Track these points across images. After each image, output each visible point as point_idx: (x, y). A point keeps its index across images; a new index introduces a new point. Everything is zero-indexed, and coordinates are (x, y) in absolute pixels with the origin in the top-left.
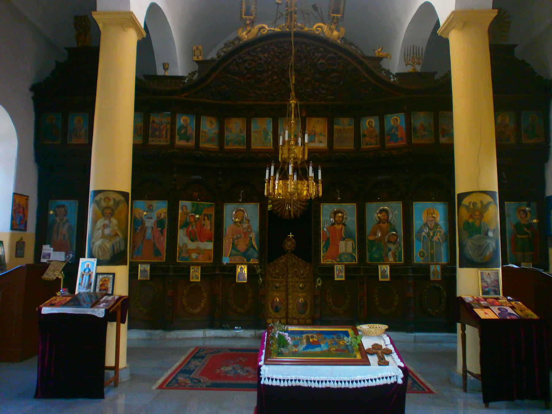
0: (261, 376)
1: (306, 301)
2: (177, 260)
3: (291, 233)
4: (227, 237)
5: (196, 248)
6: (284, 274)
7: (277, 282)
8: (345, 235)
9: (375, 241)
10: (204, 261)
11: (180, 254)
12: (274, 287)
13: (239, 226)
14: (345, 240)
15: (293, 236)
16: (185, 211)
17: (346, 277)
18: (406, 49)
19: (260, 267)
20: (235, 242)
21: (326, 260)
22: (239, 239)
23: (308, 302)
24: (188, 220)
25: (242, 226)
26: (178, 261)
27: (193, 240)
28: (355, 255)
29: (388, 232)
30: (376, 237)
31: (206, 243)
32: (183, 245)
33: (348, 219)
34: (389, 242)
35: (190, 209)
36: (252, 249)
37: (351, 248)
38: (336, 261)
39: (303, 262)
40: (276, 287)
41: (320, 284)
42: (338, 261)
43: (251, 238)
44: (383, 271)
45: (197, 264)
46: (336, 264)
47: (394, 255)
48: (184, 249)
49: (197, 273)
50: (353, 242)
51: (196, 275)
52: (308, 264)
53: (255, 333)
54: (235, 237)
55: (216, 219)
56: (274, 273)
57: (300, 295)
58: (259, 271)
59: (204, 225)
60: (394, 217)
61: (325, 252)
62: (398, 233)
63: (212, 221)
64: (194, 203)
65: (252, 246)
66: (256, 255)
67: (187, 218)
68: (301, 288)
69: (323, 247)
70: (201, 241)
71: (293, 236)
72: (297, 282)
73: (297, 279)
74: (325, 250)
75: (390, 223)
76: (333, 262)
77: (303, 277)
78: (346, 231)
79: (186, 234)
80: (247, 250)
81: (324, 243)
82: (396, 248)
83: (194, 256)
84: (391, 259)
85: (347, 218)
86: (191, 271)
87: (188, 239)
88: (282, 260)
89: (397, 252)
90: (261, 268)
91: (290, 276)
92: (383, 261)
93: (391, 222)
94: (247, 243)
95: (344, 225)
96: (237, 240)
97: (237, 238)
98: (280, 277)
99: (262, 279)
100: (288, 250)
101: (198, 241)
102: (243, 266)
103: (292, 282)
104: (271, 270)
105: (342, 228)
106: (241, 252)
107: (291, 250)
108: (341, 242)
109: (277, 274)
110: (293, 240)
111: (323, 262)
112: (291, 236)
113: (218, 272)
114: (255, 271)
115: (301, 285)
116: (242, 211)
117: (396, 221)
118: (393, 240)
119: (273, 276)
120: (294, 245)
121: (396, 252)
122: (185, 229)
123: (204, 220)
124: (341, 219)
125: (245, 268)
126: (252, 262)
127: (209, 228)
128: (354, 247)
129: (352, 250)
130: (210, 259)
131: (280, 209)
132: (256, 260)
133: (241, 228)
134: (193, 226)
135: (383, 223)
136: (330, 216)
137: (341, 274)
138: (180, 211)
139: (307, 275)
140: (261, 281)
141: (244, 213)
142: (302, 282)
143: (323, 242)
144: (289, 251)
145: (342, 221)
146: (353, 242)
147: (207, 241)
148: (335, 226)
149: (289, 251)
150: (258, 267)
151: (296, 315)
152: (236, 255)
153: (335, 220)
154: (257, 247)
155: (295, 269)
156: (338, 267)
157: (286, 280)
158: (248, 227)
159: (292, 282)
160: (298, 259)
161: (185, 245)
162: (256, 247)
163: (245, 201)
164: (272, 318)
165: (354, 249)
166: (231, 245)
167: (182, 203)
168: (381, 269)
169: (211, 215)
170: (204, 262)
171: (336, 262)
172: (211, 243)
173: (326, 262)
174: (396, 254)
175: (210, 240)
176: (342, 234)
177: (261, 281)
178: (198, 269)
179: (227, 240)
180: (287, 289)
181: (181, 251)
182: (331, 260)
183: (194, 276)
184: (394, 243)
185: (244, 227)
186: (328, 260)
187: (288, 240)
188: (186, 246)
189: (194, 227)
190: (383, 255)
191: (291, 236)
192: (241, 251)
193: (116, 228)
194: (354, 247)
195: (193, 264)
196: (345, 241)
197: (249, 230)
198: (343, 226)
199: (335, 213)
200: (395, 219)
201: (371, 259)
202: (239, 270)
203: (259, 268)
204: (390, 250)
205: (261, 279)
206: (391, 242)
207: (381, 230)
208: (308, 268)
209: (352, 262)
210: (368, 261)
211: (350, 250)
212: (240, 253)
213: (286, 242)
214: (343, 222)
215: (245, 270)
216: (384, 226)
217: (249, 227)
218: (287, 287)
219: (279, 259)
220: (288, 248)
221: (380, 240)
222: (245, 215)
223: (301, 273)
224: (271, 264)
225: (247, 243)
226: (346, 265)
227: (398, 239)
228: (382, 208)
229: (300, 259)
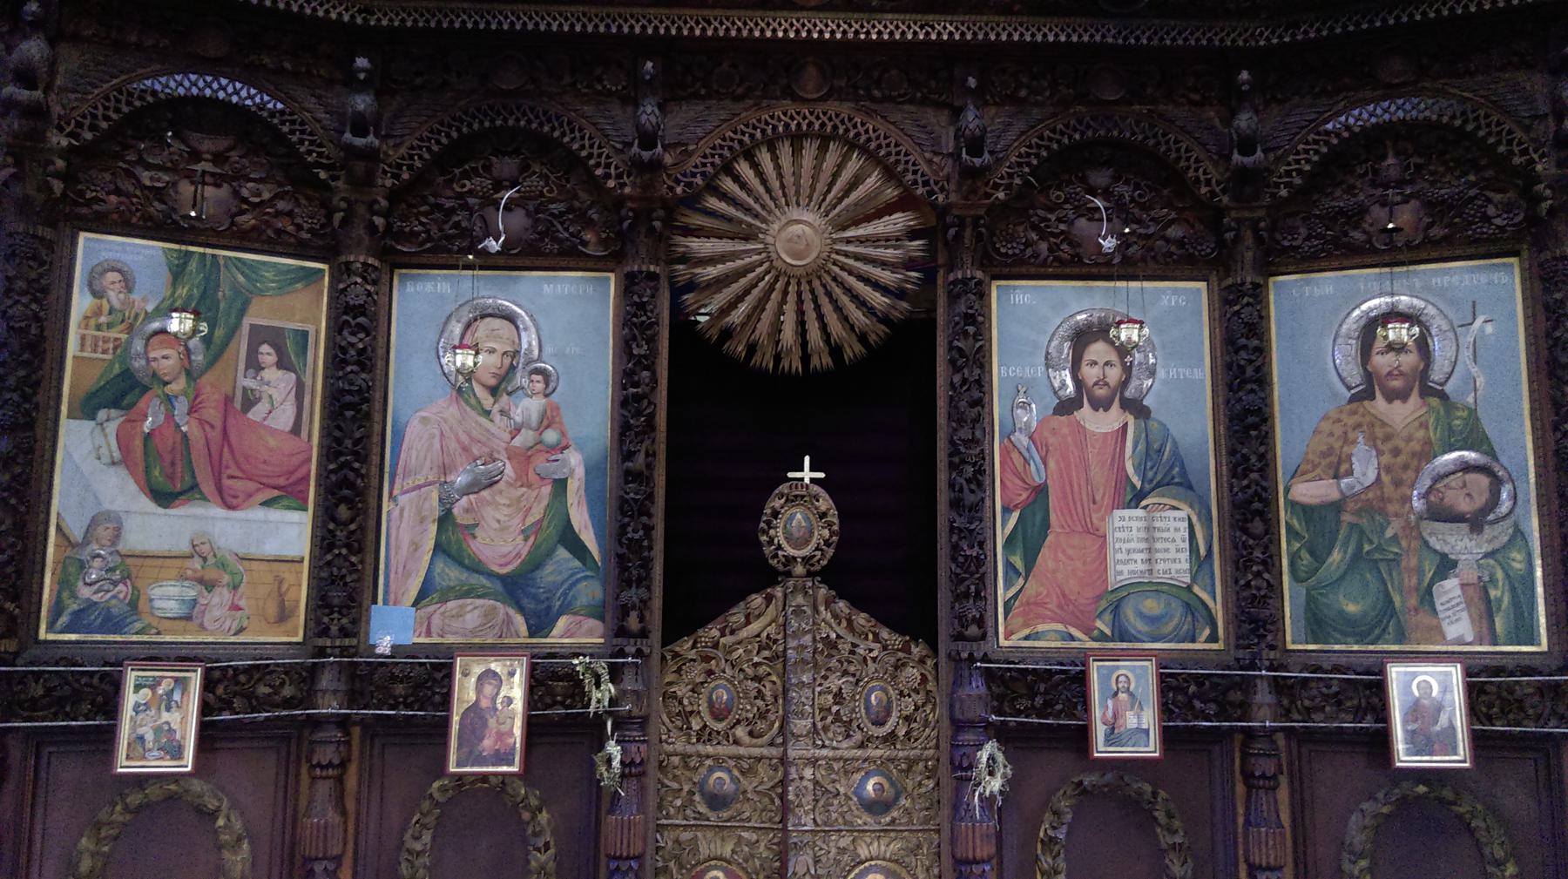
2: (43, 627)
3: (807, 459)
4: (410, 483)
5: (185, 547)
6: (762, 715)
7: (719, 762)
8: (1141, 470)
9: (1337, 507)
10: (240, 631)
11: (64, 583)
12: (697, 798)
13: (487, 413)
14: (1144, 503)
15: (821, 475)
16: (115, 297)
17: (1169, 737)
20: (456, 511)
21: (1026, 625)
22: (485, 493)
24: (138, 364)
26: (51, 637)
27: (164, 498)
28: (1205, 596)
29: (1428, 454)
30: (1345, 482)
31: (260, 513)
32: (94, 523)
33: (1161, 373)
34: (1441, 514)
35: (149, 293)
36: (562, 553)
37: (1185, 555)
38: (1088, 631)
39: (885, 634)
40: (717, 801)
41: (995, 784)
42: (1103, 637)
43: (561, 486)
44: (1417, 702)
45: (183, 657)
46: (1104, 655)
47: (1485, 610)
48: (94, 547)
49: (172, 718)
50: (1195, 519)
51: (162, 731)
52: (917, 650)
54: (460, 480)
55: (337, 359)
56: (704, 708)
57: (863, 852)
58: (601, 696)
59: (250, 401)
60: (1466, 354)
61: (1018, 574)
62: (1504, 459)
63: (308, 380)
64: (189, 254)
65: (569, 539)
66: (591, 591)
67: (129, 343)
68: (876, 807)
69: (1009, 542)
70: (229, 502)
71: (821, 475)
72: (848, 767)
73: (846, 749)
74: (1018, 561)
75: (1443, 396)
76: (1072, 638)
77: (882, 731)
79: (117, 455)
80: (535, 562)
81: (1015, 515)
82: (1487, 555)
83: (167, 597)
84: (1459, 628)
85: (1152, 373)
86: (130, 698)
87: (132, 486)
88: (755, 627)
89: (1500, 575)
90: (616, 674)
91: (801, 725)
92: (1401, 638)
93: (1448, 388)
94: (531, 520)
95: (1136, 408)
96: (472, 497)
97: (473, 488)
98: (740, 732)
99: (624, 752)
100: (790, 560)
101: (205, 499)
102: (496, 666)
103: (813, 762)
104: (682, 690)
105: (1125, 426)
106: (490, 575)
107: (806, 560)
108: (1118, 513)
110: (825, 503)
111: (1006, 638)
112: (807, 475)
113: (329, 707)
114: (577, 692)
115: (870, 787)
116: (510, 318)
117: (1480, 381)
118: (1464, 506)
119: (696, 725)
120: (826, 533)
121: (1493, 580)
122: (113, 421)
123: (254, 365)
124: (1114, 374)
125: (512, 674)
126: (563, 633)
127: (284, 418)
128: (1203, 552)
129: (1186, 566)
130: (283, 616)
131: (743, 308)
132: (593, 623)
133: (499, 427)
134: (169, 400)
135: (1391, 396)
136: (1048, 353)
137: (1131, 721)
138: (81, 303)
139: (908, 719)
140: (616, 763)
142: (882, 767)
143: (1007, 510)
144: (799, 569)
145: (1124, 384)
146: (1195, 519)
147: (267, 504)
149: (799, 569)
150: (602, 667)
152: (469, 593)
153: (1078, 382)
154: (599, 537)
155: (835, 682)
156: (1415, 675)
157: (774, 752)
158: (543, 415)
159: (813, 762)
160: (849, 621)
161: (108, 523)
162: (589, 538)
163: (520, 256)
165: (1200, 563)
166: (434, 528)
167: (91, 248)
168: (1104, 679)
169: (305, 334)
170: (241, 638)
171: (1094, 640)
172: (295, 516)
173: (1027, 638)
174: (1493, 593)
175: (287, 494)
176: (1124, 468)
177: (616, 763)
178: (182, 683)
179: (403, 499)
180: (786, 809)
181: (73, 568)
182: (1060, 627)
183: (149, 737)
184: (1476, 523)
187: (792, 500)
188: (117, 535)
189: (181, 407)
190: (1397, 599)
191: (807, 475)
192: (496, 569)
194: (1203, 552)
195: (154, 656)
196: (1145, 507)
197: (551, 436)
198: (1131, 420)
199: (1082, 338)
200: (1474, 370)
201: (1317, 625)
202: (465, 691)
204: (1446, 566)
205: (613, 749)
206: (1455, 518)
207: (1380, 436)
208: (912, 673)
209: (1193, 641)
210: (1294, 638)
211: (1175, 564)
212: (484, 581)
213: (775, 514)
214: (1130, 392)
215: (516, 690)
216: (1402, 414)
218: (783, 797)
219: (736, 616)
220: (792, 552)
221: (1374, 505)
222: (525, 346)
223: (868, 707)
224: (684, 646)
225: (536, 514)
226: (1164, 662)
227: (1504, 496)
228: (1357, 313)
229: (861, 619)
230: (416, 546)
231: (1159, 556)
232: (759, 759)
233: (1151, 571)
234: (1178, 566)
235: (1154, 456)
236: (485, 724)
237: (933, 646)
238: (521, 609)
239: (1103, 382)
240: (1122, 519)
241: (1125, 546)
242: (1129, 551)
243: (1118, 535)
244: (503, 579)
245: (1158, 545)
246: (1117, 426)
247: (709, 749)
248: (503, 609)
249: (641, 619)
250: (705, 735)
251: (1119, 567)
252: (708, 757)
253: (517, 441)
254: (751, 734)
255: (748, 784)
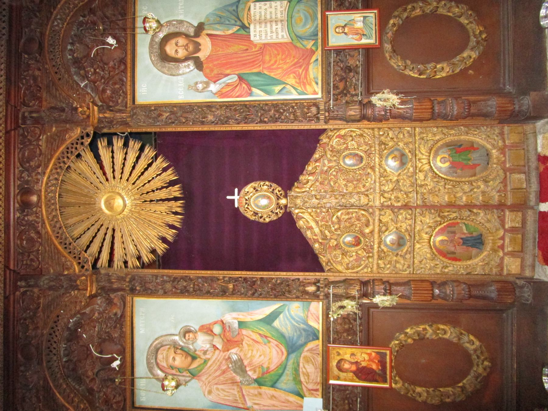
0: (200, 47)
1: (447, 145)
3: (228, 197)
13: (206, 361)
14: (247, 25)
18: (100, 223)
19: (334, 301)
22: (246, 363)
23: (449, 139)
25: (205, 352)
38: (313, 52)
39: (316, 156)
40: (400, 242)
52: (324, 139)
53: (141, 378)
58: (350, 306)
65: (269, 320)
68: (402, 159)
69: (268, 93)
74: (278, 88)
78: (219, 23)
81: (254, 90)
95: (200, 28)
100: (279, 206)
106: (287, 359)
108: (252, 38)
109: (357, 242)
111: (317, 94)
112: (236, 197)
141: (162, 346)
143: (250, 94)
144: (283, 201)
145: (187, 36)
148: (202, 59)
149: (283, 201)
151: (494, 179)
152: (296, 370)
164: (502, 259)
166: (265, 390)
173: (317, 83)
178: (315, 93)
185: (208, 346)
186: (312, 76)
193: (90, 258)
197: (217, 329)
198: (205, 32)
203: (339, 304)
214: (191, 32)
217: (207, 330)
218: (400, 208)
219: (309, 234)
224: (323, 259)
230: (273, 397)
231: (274, 16)
232: (380, 221)
233: (281, 21)
234: (279, 7)
235: (223, 20)
236: (364, 368)
237: (322, 131)
238: (305, 344)
239: (186, 47)
240: (255, 36)
241: (269, 34)
242: (272, 32)
243: (263, 38)
244: (289, 354)
245: (268, 17)
246: (208, 39)
247: (376, 246)
248: (305, 352)
249: (310, 284)
250: (369, 249)
251: (280, 37)
252: (379, 247)
253: (220, 346)
254: (367, 225)
255: (392, 227)
